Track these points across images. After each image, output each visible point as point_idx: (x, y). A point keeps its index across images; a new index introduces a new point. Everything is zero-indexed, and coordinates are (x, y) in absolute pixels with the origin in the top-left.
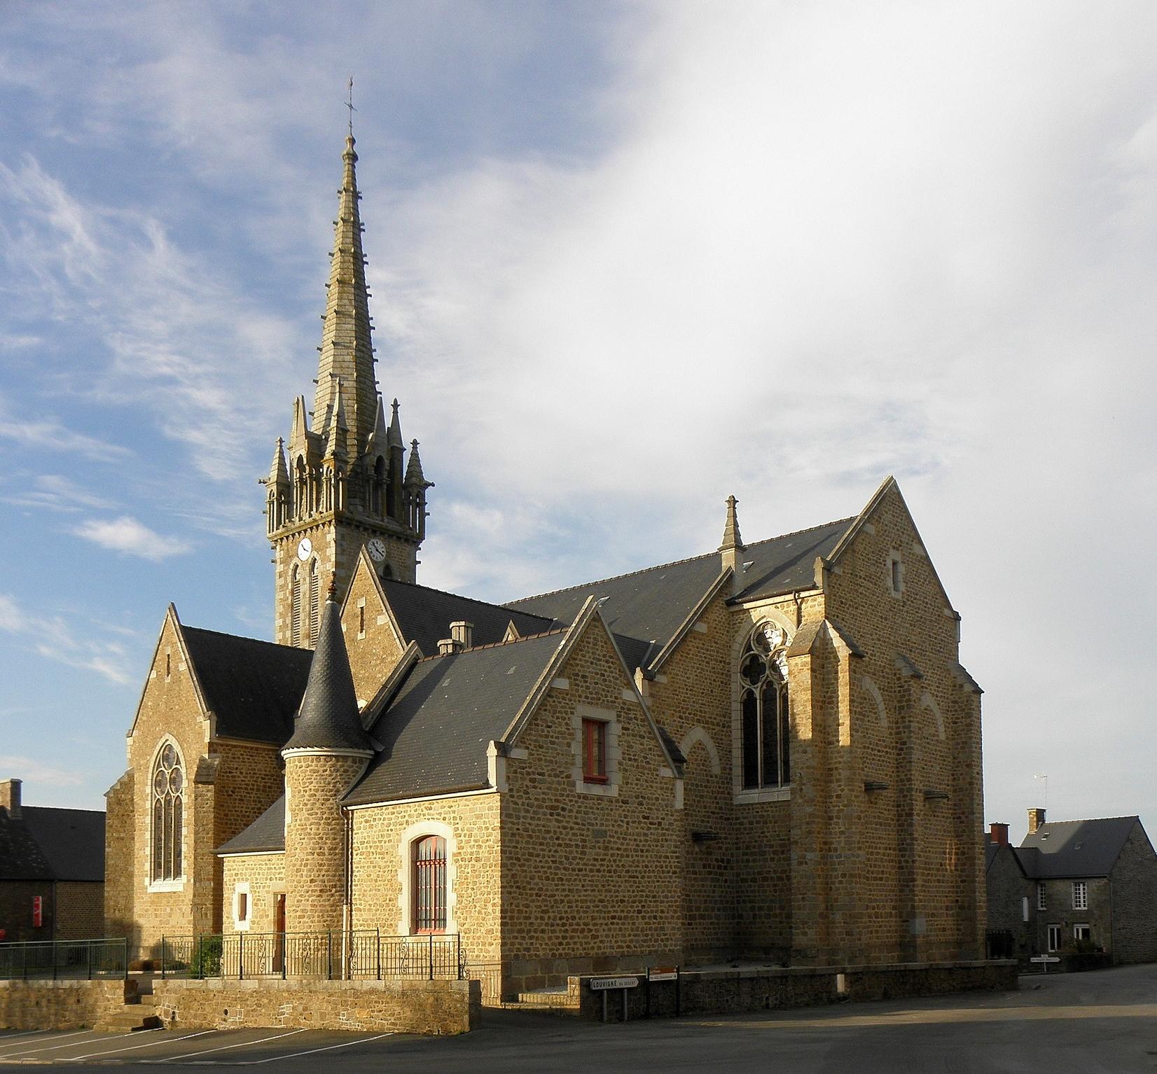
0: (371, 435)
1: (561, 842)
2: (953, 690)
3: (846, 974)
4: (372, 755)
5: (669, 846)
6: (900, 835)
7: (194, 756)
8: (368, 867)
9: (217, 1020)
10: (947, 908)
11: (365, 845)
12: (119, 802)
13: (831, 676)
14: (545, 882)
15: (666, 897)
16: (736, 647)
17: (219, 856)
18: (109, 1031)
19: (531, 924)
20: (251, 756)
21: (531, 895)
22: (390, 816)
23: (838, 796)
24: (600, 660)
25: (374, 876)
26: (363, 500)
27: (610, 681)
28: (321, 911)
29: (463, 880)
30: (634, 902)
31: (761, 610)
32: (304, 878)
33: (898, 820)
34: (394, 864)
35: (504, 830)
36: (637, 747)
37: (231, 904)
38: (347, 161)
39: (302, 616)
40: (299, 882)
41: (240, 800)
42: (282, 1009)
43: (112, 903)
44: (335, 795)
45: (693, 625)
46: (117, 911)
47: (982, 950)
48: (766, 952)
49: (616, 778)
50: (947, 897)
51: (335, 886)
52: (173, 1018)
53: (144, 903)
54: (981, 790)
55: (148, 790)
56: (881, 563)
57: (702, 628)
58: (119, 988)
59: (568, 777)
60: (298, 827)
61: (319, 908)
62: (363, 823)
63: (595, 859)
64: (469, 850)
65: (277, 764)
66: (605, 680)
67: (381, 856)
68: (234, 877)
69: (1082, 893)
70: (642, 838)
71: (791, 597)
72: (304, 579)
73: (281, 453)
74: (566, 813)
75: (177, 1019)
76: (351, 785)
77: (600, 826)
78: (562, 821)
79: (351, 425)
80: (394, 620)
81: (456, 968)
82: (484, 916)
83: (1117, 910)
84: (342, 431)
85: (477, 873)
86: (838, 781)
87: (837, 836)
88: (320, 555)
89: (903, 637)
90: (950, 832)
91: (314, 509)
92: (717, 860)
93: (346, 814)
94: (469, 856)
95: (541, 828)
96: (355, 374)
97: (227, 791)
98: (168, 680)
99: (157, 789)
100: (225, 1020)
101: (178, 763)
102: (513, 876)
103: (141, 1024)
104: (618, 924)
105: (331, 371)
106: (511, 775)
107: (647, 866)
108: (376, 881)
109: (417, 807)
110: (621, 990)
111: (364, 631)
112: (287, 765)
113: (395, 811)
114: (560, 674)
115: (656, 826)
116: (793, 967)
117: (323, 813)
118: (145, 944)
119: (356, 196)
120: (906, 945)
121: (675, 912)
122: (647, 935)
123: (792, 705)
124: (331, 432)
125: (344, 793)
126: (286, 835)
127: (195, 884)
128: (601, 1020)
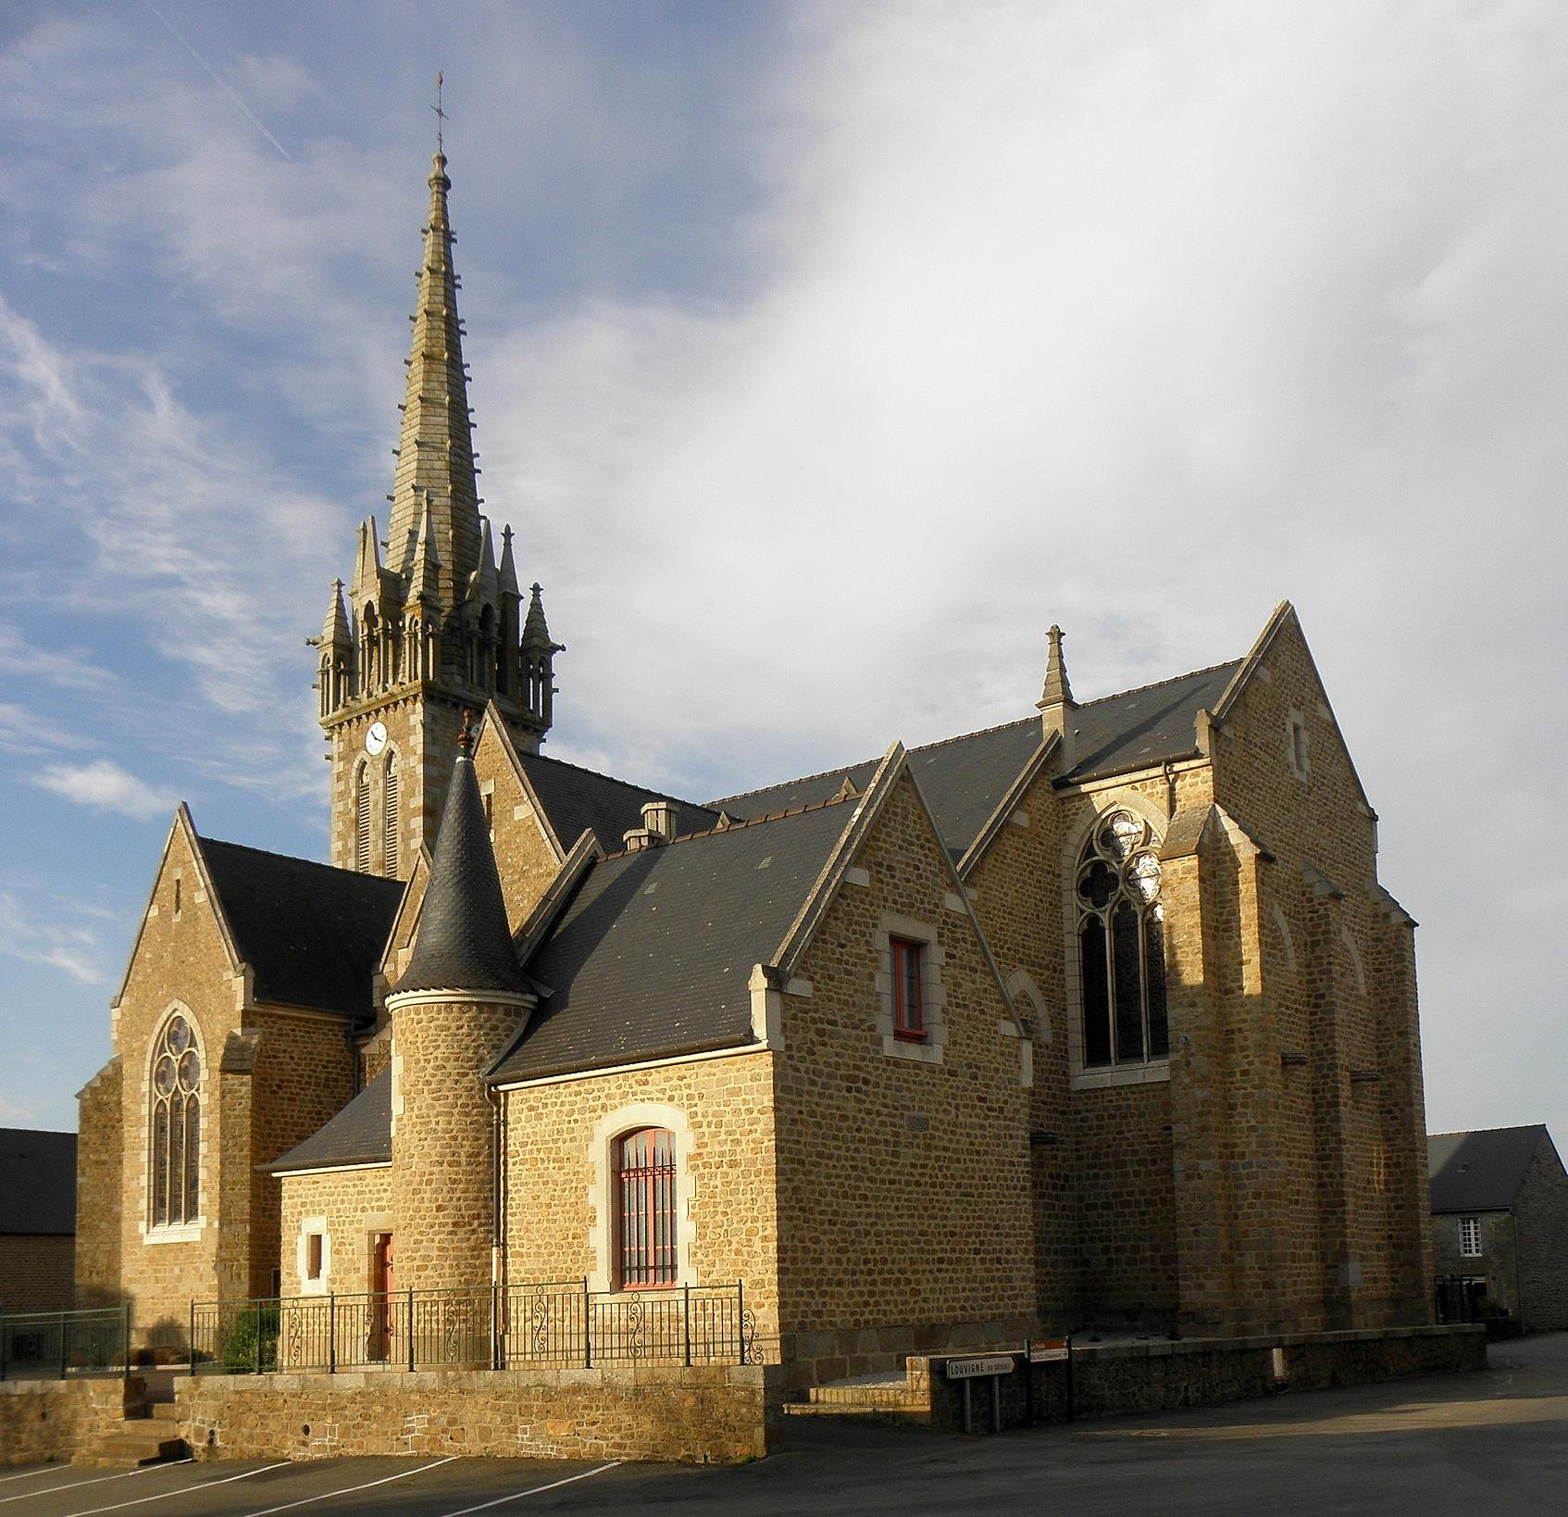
0: (474, 574)
1: (863, 1135)
2: (1373, 922)
3: (1284, 1348)
4: (533, 1003)
5: (1015, 1146)
6: (1319, 1136)
7: (218, 1032)
8: (535, 1184)
9: (290, 1443)
10: (1378, 1247)
11: (529, 1147)
12: (99, 1107)
13: (1228, 890)
14: (842, 1201)
15: (1013, 1227)
16: (1070, 850)
17: (274, 1175)
18: (99, 1466)
19: (823, 1270)
20: (308, 1032)
21: (822, 1223)
22: (573, 1098)
23: (1245, 1073)
24: (911, 844)
25: (544, 1199)
26: (463, 667)
27: (927, 878)
28: (456, 1258)
29: (707, 1199)
30: (969, 1235)
31: (1105, 794)
32: (427, 1204)
33: (1315, 1113)
34: (581, 1176)
35: (780, 1114)
36: (967, 986)
37: (294, 1252)
38: (435, 188)
39: (372, 836)
40: (418, 1210)
41: (289, 1099)
42: (409, 1422)
43: (87, 1262)
44: (477, 1067)
45: (1011, 814)
46: (94, 1275)
47: (1431, 1310)
48: (1132, 1318)
49: (940, 1034)
50: (1377, 1230)
51: (478, 1216)
52: (211, 1441)
53: (137, 1260)
54: (1419, 1070)
55: (145, 1087)
56: (1279, 727)
57: (1022, 819)
58: (115, 1391)
59: (872, 1028)
60: (415, 1119)
61: (451, 1252)
62: (525, 1111)
63: (913, 1166)
64: (717, 1148)
65: (346, 1046)
66: (920, 876)
67: (557, 1165)
68: (300, 1209)
69: (1472, 1233)
70: (978, 1132)
71: (1159, 771)
72: (376, 782)
73: (340, 600)
74: (869, 1088)
75: (219, 1443)
76: (504, 1051)
77: (919, 1110)
78: (865, 1101)
79: (445, 558)
80: (542, 811)
81: (737, 1346)
82: (746, 1257)
83: (1524, 1256)
84: (432, 567)
85: (732, 1187)
86: (1243, 1049)
87: (1244, 1135)
88: (400, 746)
89: (1310, 840)
90: (1377, 1132)
91: (391, 681)
92: (1051, 1176)
93: (495, 1098)
94: (717, 1158)
95: (834, 1111)
96: (450, 487)
97: (270, 1086)
98: (177, 918)
99: (160, 1085)
100: (304, 1444)
101: (193, 1043)
102: (795, 1190)
103: (155, 1452)
104: (947, 1271)
105: (414, 481)
106: (789, 1022)
107: (985, 1178)
108: (549, 1206)
109: (621, 1081)
110: (989, 1379)
112: (395, 1020)
113: (582, 1089)
114: (856, 861)
115: (996, 1114)
116: (1185, 1340)
117: (457, 1097)
118: (140, 1324)
119: (448, 238)
120: (1334, 1303)
121: (1026, 1252)
122: (988, 1289)
123: (1170, 934)
124: (415, 568)
125: (491, 1063)
126: (393, 1134)
127: (221, 1228)
128: (962, 1429)
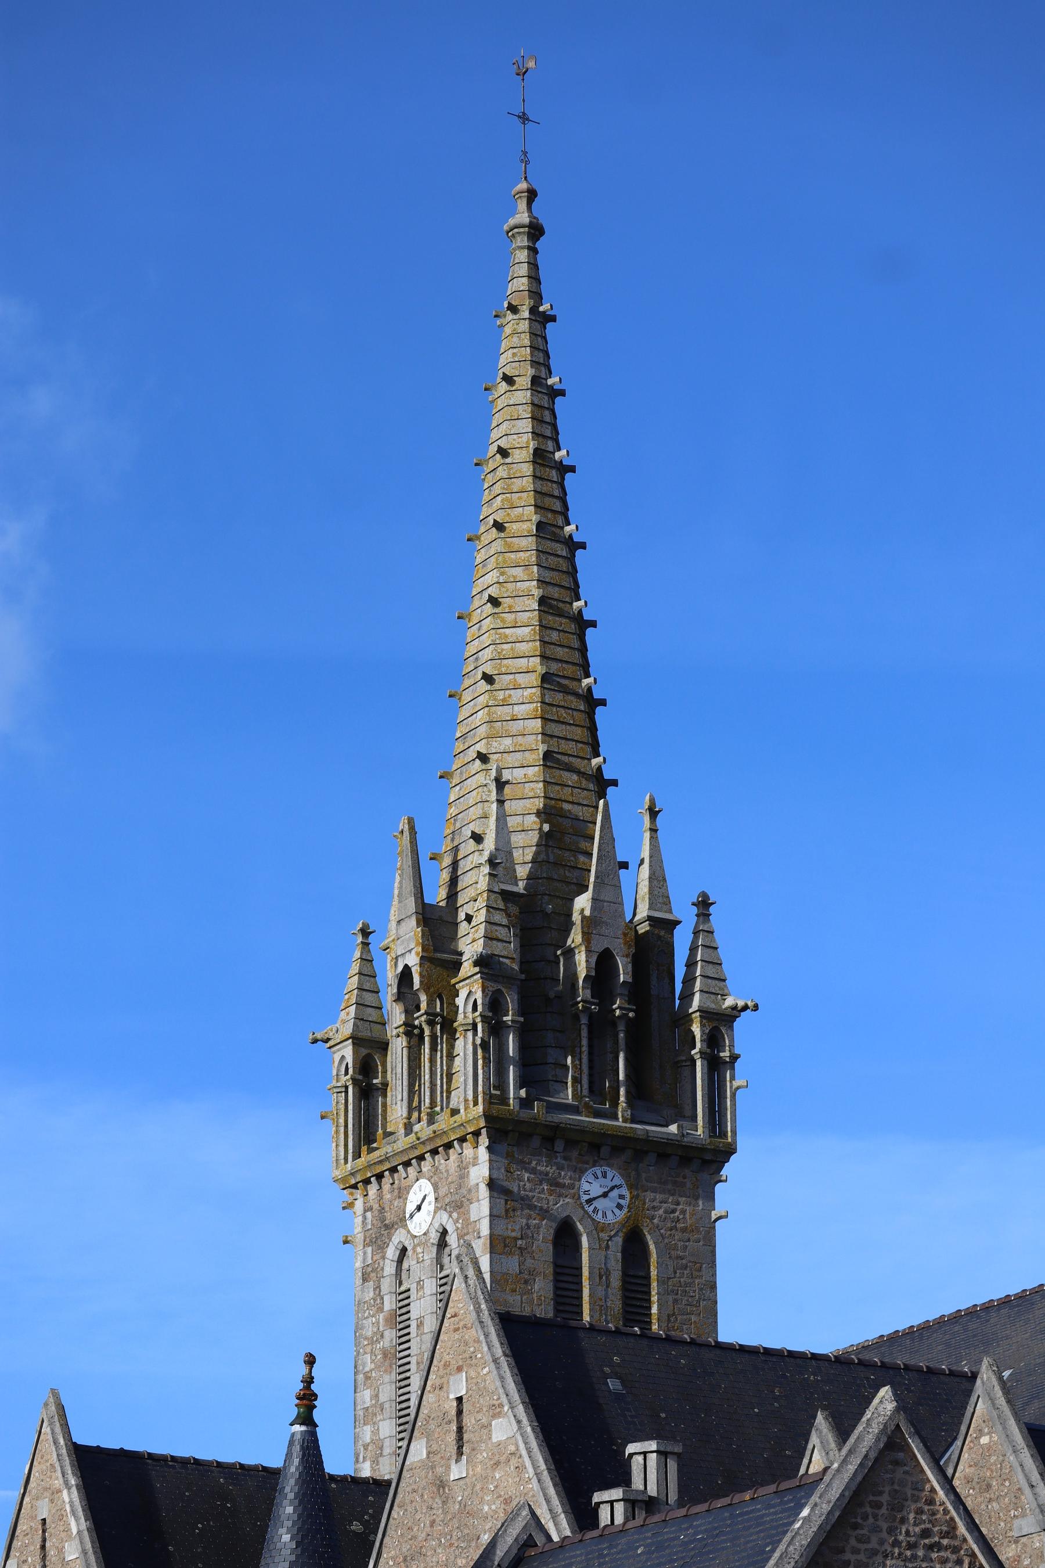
88: (456, 1221)
111: (464, 1457)
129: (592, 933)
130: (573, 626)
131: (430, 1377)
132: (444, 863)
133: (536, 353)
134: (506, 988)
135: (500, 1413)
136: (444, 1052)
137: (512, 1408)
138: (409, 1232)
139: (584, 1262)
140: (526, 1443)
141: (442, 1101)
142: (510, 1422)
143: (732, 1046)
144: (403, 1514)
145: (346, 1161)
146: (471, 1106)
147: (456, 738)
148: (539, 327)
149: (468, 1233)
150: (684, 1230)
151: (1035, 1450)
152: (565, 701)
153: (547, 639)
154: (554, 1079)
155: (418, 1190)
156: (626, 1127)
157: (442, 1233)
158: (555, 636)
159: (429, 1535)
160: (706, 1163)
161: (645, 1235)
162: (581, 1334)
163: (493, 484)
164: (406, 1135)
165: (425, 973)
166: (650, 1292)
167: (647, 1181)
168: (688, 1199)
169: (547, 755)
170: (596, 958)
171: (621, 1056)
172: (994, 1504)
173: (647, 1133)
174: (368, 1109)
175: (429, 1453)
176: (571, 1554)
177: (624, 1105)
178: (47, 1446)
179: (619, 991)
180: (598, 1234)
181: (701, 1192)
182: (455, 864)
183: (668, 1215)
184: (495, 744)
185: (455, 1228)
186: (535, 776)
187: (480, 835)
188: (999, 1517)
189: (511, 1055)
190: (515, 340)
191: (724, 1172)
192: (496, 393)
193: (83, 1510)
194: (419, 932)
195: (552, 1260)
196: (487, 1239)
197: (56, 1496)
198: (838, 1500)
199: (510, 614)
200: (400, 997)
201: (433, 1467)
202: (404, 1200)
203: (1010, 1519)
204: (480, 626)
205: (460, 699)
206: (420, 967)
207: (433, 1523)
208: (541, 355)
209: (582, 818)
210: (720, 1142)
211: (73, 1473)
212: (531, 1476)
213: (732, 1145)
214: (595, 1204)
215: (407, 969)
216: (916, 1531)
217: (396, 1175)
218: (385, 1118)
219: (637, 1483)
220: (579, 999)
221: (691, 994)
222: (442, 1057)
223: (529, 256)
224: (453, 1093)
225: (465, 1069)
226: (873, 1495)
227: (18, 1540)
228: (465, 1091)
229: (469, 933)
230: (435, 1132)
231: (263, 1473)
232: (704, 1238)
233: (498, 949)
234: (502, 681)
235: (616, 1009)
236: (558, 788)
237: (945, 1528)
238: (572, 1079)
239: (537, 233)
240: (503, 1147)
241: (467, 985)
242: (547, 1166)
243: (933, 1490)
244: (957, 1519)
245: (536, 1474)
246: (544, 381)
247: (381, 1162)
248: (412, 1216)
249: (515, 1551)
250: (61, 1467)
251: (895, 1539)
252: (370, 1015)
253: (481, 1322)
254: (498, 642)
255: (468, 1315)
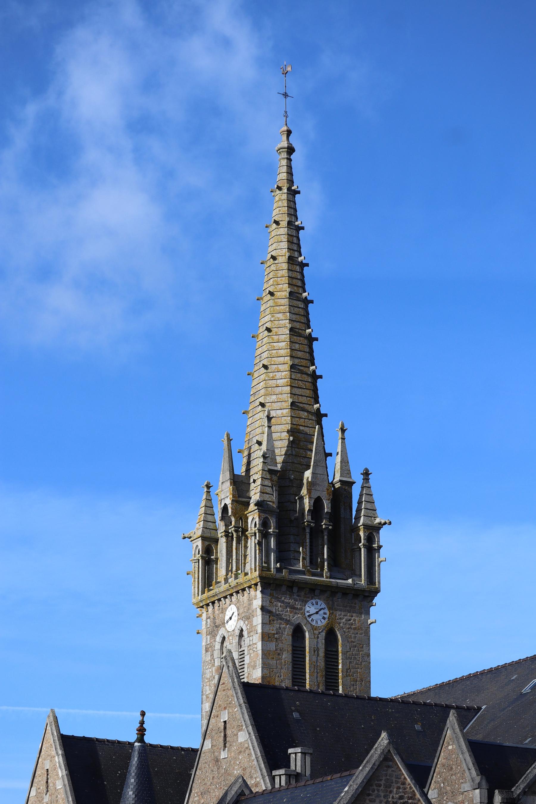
88: (247, 625)
98: (46, 799)
129: (312, 489)
130: (306, 341)
131: (213, 711)
132: (244, 454)
133: (290, 209)
134: (270, 516)
135: (242, 729)
136: (243, 545)
137: (247, 727)
138: (226, 629)
139: (306, 645)
140: (252, 744)
141: (242, 568)
142: (246, 734)
143: (379, 541)
144: (201, 773)
145: (198, 596)
146: (254, 572)
147: (251, 394)
148: (291, 197)
149: (252, 631)
150: (355, 629)
151: (471, 753)
152: (302, 377)
153: (293, 348)
154: (294, 558)
155: (230, 609)
156: (327, 581)
157: (241, 631)
158: (297, 346)
159: (212, 783)
160: (365, 597)
161: (336, 631)
162: (282, 692)
163: (269, 273)
164: (225, 584)
165: (234, 508)
166: (338, 658)
167: (338, 606)
168: (357, 614)
169: (293, 404)
170: (313, 501)
171: (326, 547)
172: (454, 777)
173: (337, 583)
174: (209, 570)
175: (212, 746)
176: (258, 800)
177: (327, 570)
178: (49, 735)
179: (324, 516)
180: (313, 631)
181: (363, 611)
182: (249, 455)
183: (347, 622)
184: (268, 398)
185: (246, 628)
186: (286, 413)
187: (260, 441)
188: (456, 782)
189: (272, 548)
190: (280, 204)
191: (374, 601)
192: (271, 229)
193: (65, 766)
194: (231, 488)
195: (291, 644)
196: (260, 634)
197: (53, 759)
198: (361, 783)
199: (276, 336)
200: (223, 518)
201: (214, 752)
202: (224, 614)
203: (460, 784)
204: (262, 341)
205: (253, 376)
206: (232, 505)
207: (213, 777)
208: (292, 210)
209: (309, 434)
210: (372, 587)
211: (60, 749)
212: (254, 759)
213: (378, 589)
214: (312, 617)
215: (226, 506)
216: (397, 797)
217: (221, 602)
218: (217, 574)
219: (293, 767)
220: (305, 520)
221: (359, 517)
222: (242, 547)
223: (287, 162)
224: (247, 564)
225: (251, 554)
226: (377, 781)
227: (36, 778)
228: (251, 565)
229: (253, 489)
230: (237, 583)
231: (150, 747)
232: (365, 632)
233: (267, 497)
234: (272, 368)
235: (323, 525)
236: (297, 419)
237: (410, 795)
238: (302, 558)
239: (291, 151)
240: (269, 591)
241: (252, 514)
242: (289, 600)
243: (405, 778)
244: (416, 791)
245: (256, 758)
246: (294, 223)
247: (213, 596)
248: (227, 622)
249: (235, 798)
250: (55, 746)
251: (387, 800)
252: (210, 526)
253: (234, 687)
254: (270, 349)
255: (229, 684)
